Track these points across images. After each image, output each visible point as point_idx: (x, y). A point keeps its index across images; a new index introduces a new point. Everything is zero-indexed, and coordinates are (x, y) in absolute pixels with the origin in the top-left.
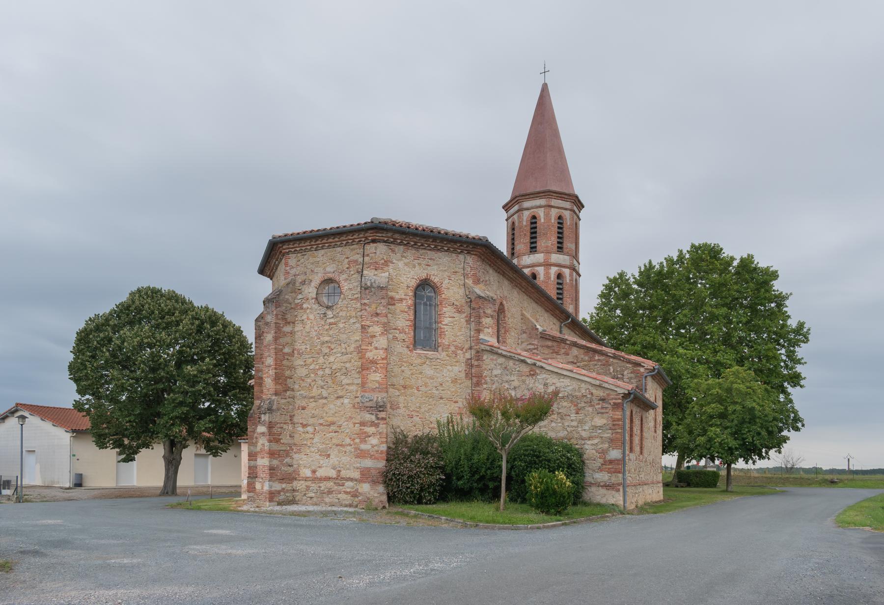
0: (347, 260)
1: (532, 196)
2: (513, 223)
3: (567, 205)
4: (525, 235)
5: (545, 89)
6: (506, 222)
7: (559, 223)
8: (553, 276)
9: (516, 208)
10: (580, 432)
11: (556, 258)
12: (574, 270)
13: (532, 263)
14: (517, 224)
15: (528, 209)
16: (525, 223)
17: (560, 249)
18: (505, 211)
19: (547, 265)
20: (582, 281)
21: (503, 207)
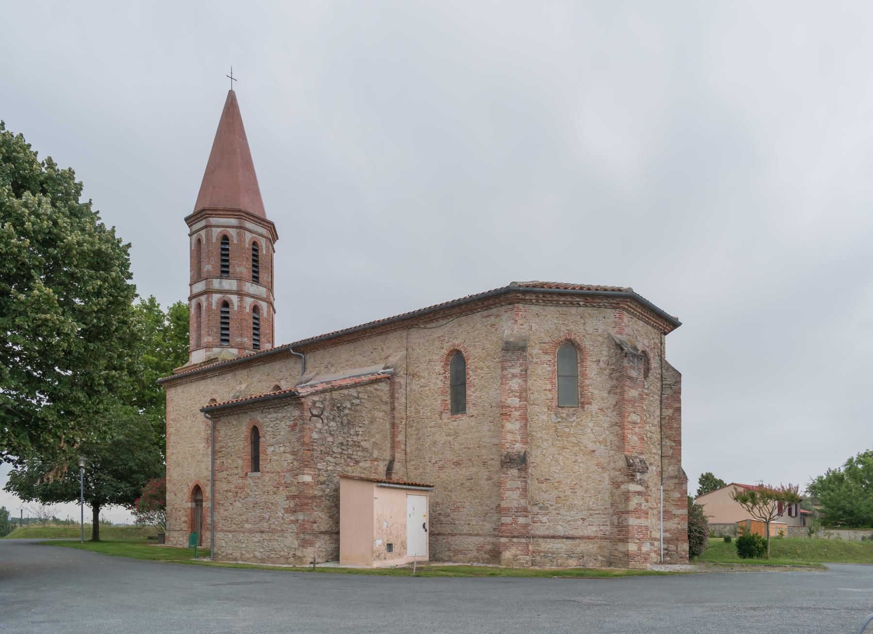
0: (638, 337)
1: (256, 219)
3: (264, 231)
4: (247, 258)
5: (231, 109)
6: (189, 238)
7: (254, 249)
8: (247, 244)
9: (203, 223)
10: (757, 506)
11: (251, 288)
12: (271, 304)
13: (255, 293)
14: (204, 241)
15: (218, 226)
16: (247, 246)
17: (256, 279)
18: (188, 224)
19: (240, 294)
20: (276, 316)
21: (186, 219)
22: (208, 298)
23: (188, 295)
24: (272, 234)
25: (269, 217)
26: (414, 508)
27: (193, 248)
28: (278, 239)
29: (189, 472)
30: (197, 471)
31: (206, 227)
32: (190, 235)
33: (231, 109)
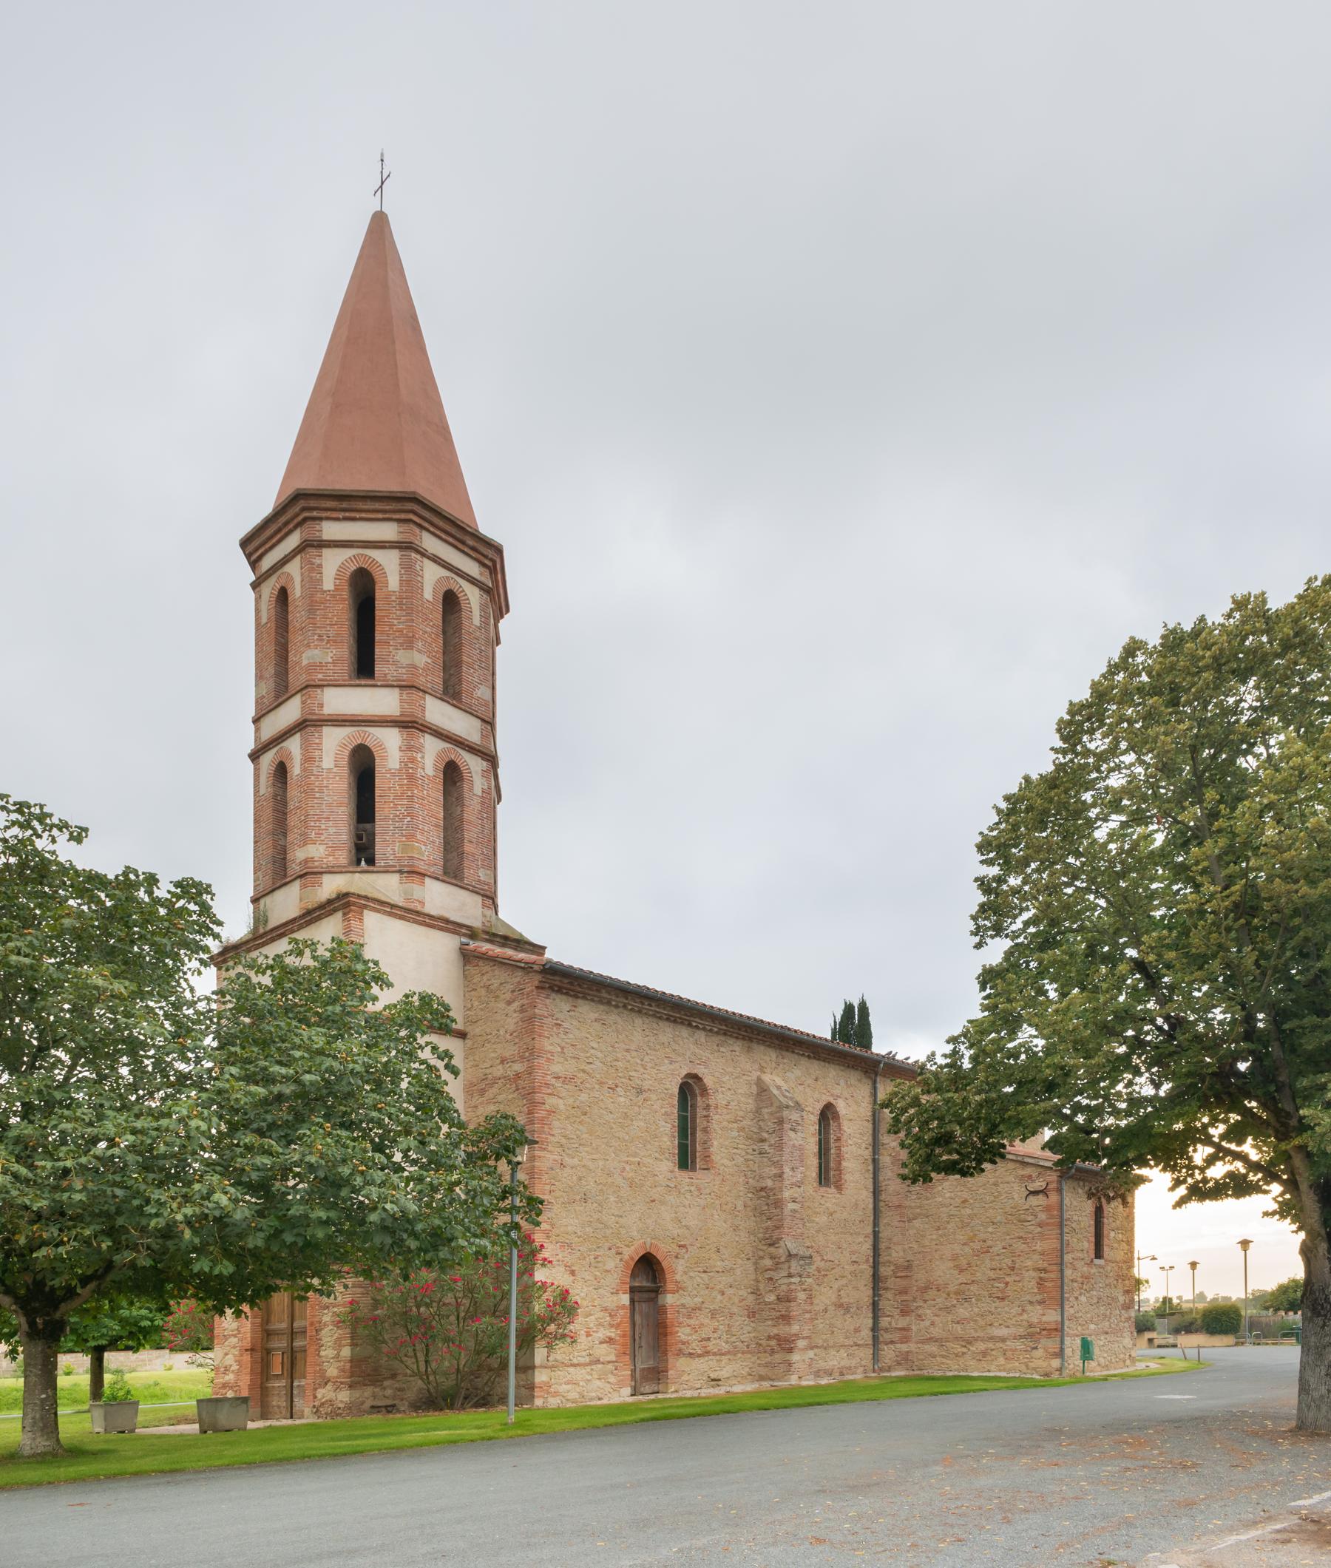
3: (472, 568)
5: (379, 225)
6: (251, 766)
12: (491, 759)
18: (248, 556)
19: (410, 724)
22: (306, 747)
24: (495, 581)
25: (486, 528)
26: (1154, 1259)
27: (264, 620)
28: (508, 611)
29: (622, 1221)
30: (649, 1221)
31: (301, 726)
32: (255, 586)
33: (379, 225)
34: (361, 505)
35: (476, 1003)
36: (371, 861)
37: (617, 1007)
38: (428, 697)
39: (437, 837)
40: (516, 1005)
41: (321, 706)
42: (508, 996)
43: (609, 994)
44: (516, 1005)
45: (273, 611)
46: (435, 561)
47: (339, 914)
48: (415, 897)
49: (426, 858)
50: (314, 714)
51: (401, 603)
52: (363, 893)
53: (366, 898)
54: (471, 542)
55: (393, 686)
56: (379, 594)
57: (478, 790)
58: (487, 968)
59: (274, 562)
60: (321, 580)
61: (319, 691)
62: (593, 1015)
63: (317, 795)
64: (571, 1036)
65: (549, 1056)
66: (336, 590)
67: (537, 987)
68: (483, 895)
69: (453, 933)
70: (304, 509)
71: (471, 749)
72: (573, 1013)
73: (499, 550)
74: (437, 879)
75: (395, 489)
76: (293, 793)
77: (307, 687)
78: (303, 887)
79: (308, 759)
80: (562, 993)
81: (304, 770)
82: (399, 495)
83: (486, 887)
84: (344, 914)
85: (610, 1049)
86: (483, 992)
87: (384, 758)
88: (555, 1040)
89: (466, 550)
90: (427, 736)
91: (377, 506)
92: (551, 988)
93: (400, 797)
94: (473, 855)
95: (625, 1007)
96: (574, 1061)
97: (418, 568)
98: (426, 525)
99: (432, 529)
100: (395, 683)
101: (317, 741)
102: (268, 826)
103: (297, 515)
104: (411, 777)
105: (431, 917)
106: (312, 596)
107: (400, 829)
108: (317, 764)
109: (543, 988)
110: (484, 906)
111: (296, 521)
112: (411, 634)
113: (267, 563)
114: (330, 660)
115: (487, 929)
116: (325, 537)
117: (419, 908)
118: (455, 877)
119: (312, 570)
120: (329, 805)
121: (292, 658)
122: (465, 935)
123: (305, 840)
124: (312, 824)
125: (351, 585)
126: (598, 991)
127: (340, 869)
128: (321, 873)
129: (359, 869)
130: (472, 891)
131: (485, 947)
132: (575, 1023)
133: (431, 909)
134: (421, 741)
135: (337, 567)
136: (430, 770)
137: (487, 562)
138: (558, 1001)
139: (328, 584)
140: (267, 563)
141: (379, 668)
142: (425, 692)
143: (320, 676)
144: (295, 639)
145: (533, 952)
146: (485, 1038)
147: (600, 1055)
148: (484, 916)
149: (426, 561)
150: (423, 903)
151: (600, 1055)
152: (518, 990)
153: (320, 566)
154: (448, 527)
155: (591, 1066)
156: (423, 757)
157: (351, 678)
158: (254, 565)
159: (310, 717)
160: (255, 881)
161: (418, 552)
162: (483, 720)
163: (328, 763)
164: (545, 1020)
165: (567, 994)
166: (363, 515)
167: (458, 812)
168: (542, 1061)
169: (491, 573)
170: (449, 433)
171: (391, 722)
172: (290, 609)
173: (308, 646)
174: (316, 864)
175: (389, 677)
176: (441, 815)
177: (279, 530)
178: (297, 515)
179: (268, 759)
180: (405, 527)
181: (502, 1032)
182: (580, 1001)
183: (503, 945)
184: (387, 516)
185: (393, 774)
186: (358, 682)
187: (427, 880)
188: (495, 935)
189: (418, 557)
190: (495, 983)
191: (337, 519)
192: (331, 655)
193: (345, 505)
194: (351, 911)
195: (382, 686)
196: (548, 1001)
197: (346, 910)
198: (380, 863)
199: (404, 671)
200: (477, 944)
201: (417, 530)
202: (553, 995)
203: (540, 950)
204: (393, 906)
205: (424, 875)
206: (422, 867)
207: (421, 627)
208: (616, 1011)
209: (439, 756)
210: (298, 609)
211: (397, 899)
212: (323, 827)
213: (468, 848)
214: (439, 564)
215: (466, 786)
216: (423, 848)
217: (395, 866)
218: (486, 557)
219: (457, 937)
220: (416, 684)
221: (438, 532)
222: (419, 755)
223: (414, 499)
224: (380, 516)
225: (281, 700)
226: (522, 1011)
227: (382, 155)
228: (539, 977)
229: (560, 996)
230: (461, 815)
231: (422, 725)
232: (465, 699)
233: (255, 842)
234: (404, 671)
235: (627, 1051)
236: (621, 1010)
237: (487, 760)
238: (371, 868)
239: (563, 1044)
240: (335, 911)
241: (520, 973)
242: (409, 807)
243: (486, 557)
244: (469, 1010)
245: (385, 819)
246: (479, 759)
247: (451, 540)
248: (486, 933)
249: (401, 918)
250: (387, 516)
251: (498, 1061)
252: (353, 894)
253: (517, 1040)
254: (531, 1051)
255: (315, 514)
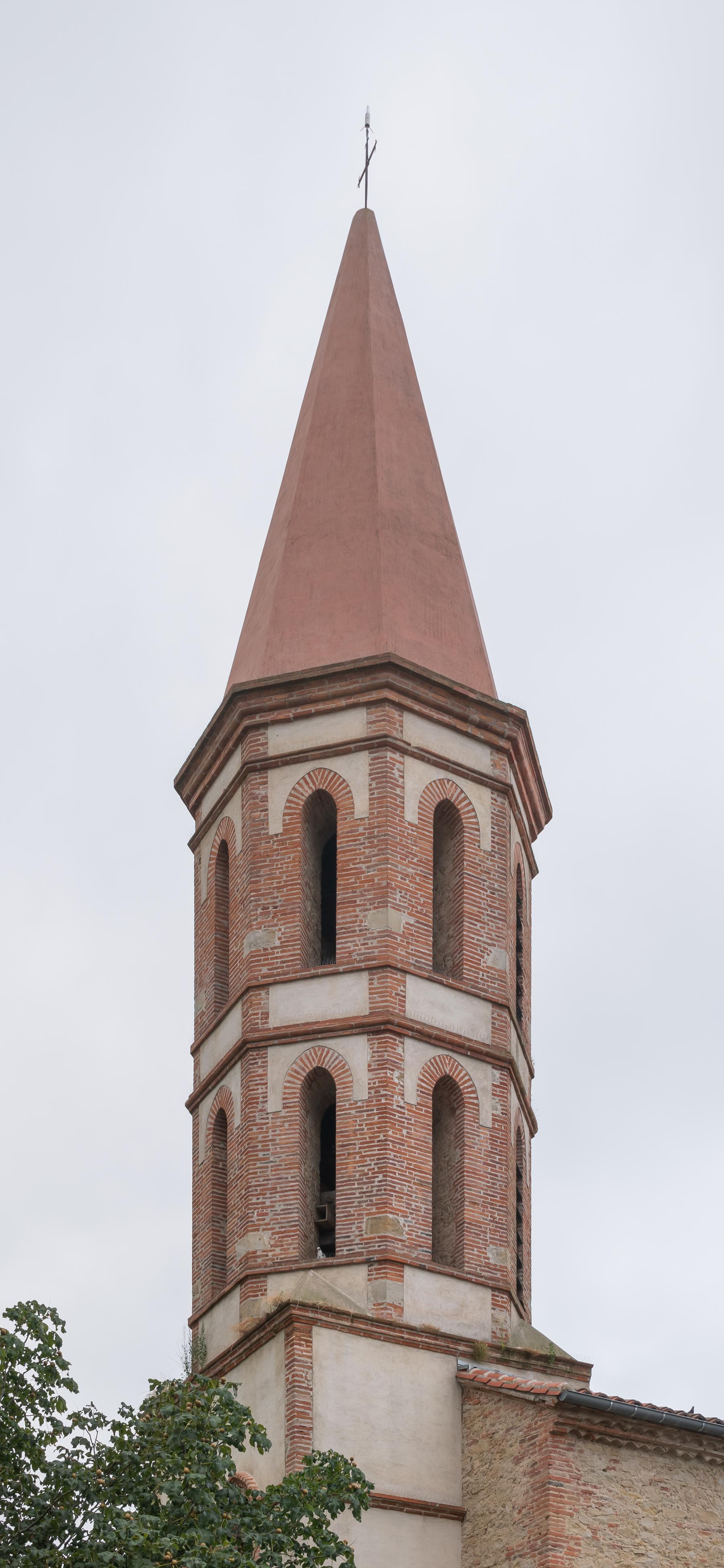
2: (224, 848)
14: (236, 1120)
16: (275, 827)
18: (186, 801)
23: (188, 1089)
27: (204, 896)
28: (549, 816)
34: (316, 692)
35: (477, 1463)
36: (330, 1250)
37: (686, 1458)
38: (409, 979)
39: (422, 1202)
40: (526, 1462)
41: (266, 1015)
42: (516, 1450)
43: (670, 1437)
44: (526, 1462)
45: (213, 879)
46: (422, 759)
47: (281, 1336)
48: (389, 1301)
49: (405, 1237)
50: (257, 1030)
51: (371, 836)
52: (310, 1302)
53: (314, 1307)
54: (476, 716)
55: (359, 970)
56: (342, 828)
57: (486, 1118)
58: (490, 1406)
59: (212, 807)
60: (265, 822)
61: (263, 993)
62: (646, 1475)
63: (261, 1155)
64: (609, 1511)
65: (572, 1544)
66: (286, 831)
67: (553, 1433)
68: (494, 1289)
69: (446, 1352)
70: (245, 715)
71: (477, 1053)
72: (611, 1473)
73: (520, 720)
74: (422, 1268)
75: (363, 655)
76: (234, 1155)
77: (248, 989)
78: (244, 1298)
79: (250, 1101)
80: (593, 1440)
81: (245, 1118)
82: (366, 663)
83: (498, 1275)
84: (288, 1335)
85: (675, 1530)
86: (485, 1444)
87: (348, 1086)
88: (583, 1517)
89: (470, 730)
90: (408, 1042)
91: (339, 687)
92: (575, 1433)
93: (367, 1144)
94: (478, 1224)
95: (699, 1457)
96: (613, 1552)
97: (397, 774)
98: (408, 702)
99: (417, 707)
100: (362, 965)
101: (260, 1071)
102: (207, 1210)
103: (237, 726)
104: (384, 1111)
105: (411, 1329)
106: (255, 847)
107: (369, 1193)
108: (260, 1106)
109: (562, 1434)
110: (495, 1305)
111: (235, 736)
112: (384, 883)
113: (206, 808)
114: (277, 943)
115: (497, 1342)
116: (272, 752)
117: (395, 1317)
118: (453, 1264)
119: (254, 808)
120: (276, 1168)
121: (233, 948)
122: (464, 1355)
123: (248, 1226)
124: (254, 1200)
125: (306, 821)
126: (652, 1433)
127: (288, 1266)
128: (266, 1274)
129: (314, 1264)
130: (477, 1283)
131: (506, 1374)
132: (617, 1489)
133: (413, 1317)
134: (399, 1050)
135: (286, 796)
136: (412, 1096)
137: (503, 743)
138: (587, 1453)
139: (275, 827)
140: (206, 808)
141: (342, 944)
142: (405, 972)
143: (265, 970)
144: (237, 916)
145: (570, 1375)
146: (488, 1519)
147: (657, 1540)
148: (495, 1321)
149: (409, 761)
150: (400, 1309)
151: (657, 1540)
152: (528, 1439)
153: (265, 799)
154: (441, 700)
155: (643, 1559)
156: (401, 1077)
157: (307, 966)
158: (194, 810)
159: (251, 1036)
160: (194, 1295)
161: (396, 748)
162: (495, 1004)
163: (274, 1103)
164: (567, 1487)
165: (600, 1441)
166: (321, 706)
167: (458, 1158)
168: (561, 1553)
169: (511, 761)
170: (456, 543)
171: (358, 1026)
172: (232, 872)
173: (249, 926)
174: (259, 1260)
175: (355, 956)
176: (429, 1166)
177: (218, 753)
178: (237, 726)
179: (208, 1106)
180: (378, 713)
181: (508, 1509)
182: (624, 1453)
183: (524, 1367)
184: (352, 700)
185: (360, 1110)
186: (320, 971)
187: (408, 1272)
188: (509, 1351)
189: (397, 756)
190: (501, 1428)
191: (287, 721)
192: (279, 934)
193: (295, 697)
194: (294, 1329)
195: (345, 972)
196: (570, 1455)
197: (289, 1330)
198: (342, 1250)
199: (375, 943)
200: (480, 1367)
201: (395, 713)
202: (580, 1445)
203: (582, 1370)
204: (355, 1317)
205: (402, 1264)
206: (399, 1251)
207: (400, 867)
208: (685, 1465)
209: (425, 1071)
210: (240, 871)
211: (365, 1307)
212: (268, 1203)
213: (471, 1213)
214: (428, 761)
215: (468, 1114)
216: (402, 1220)
217: (361, 1254)
218: (500, 735)
219: (452, 1358)
220: (392, 962)
221: (426, 711)
222: (396, 1074)
223: (390, 665)
224: (343, 702)
225: (220, 1015)
226: (533, 1473)
227: (367, 116)
228: (553, 1416)
229: (590, 1445)
230: (461, 1162)
231: (399, 1025)
232: (467, 973)
233: (194, 1236)
234: (375, 943)
235: (705, 1532)
236: (694, 1463)
237: (502, 1068)
238: (330, 1261)
239: (595, 1525)
240: (276, 1331)
241: (530, 1412)
242: (382, 1158)
243: (500, 735)
244: (469, 1474)
245: (349, 1182)
246: (489, 1067)
247: (446, 719)
248: (497, 1348)
249: (368, 1334)
250: (352, 700)
251: (504, 1556)
252: (295, 1303)
253: (527, 1521)
254: (543, 1536)
255: (258, 719)
